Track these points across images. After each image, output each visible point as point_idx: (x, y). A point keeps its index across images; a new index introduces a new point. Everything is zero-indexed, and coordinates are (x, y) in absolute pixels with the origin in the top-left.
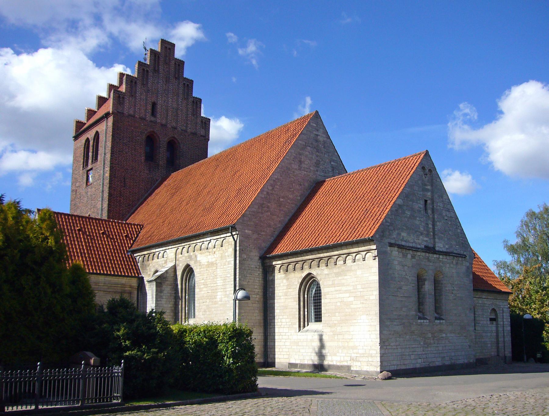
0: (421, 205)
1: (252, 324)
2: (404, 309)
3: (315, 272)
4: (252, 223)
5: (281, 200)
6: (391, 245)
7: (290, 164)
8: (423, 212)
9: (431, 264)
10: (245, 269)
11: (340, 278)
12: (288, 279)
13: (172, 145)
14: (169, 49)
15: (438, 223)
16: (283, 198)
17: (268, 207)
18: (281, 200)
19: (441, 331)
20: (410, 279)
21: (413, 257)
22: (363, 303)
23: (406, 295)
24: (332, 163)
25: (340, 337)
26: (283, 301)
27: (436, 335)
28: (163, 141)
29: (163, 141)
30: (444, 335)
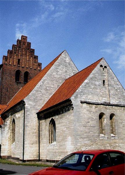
0: (101, 82)
1: (32, 143)
2: (91, 133)
3: (53, 118)
4: (33, 99)
5: (47, 88)
6: (82, 102)
7: (52, 73)
8: (102, 86)
9: (108, 110)
10: (28, 119)
11: (61, 119)
12: (46, 122)
13: (27, 74)
14: (25, 39)
15: (111, 91)
16: (48, 87)
17: (40, 91)
18: (47, 88)
19: (115, 143)
20: (94, 118)
21: (96, 107)
22: (69, 131)
23: (91, 126)
24: (73, 71)
25: (62, 147)
26: (44, 132)
27: (112, 145)
28: (23, 73)
29: (23, 73)
30: (118, 145)
